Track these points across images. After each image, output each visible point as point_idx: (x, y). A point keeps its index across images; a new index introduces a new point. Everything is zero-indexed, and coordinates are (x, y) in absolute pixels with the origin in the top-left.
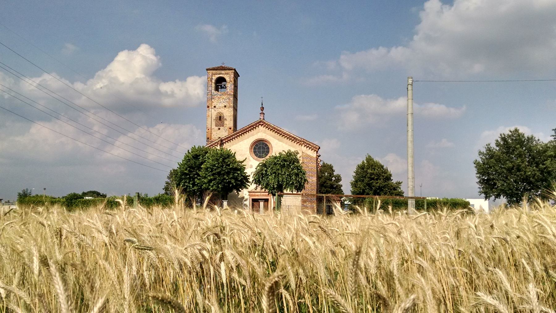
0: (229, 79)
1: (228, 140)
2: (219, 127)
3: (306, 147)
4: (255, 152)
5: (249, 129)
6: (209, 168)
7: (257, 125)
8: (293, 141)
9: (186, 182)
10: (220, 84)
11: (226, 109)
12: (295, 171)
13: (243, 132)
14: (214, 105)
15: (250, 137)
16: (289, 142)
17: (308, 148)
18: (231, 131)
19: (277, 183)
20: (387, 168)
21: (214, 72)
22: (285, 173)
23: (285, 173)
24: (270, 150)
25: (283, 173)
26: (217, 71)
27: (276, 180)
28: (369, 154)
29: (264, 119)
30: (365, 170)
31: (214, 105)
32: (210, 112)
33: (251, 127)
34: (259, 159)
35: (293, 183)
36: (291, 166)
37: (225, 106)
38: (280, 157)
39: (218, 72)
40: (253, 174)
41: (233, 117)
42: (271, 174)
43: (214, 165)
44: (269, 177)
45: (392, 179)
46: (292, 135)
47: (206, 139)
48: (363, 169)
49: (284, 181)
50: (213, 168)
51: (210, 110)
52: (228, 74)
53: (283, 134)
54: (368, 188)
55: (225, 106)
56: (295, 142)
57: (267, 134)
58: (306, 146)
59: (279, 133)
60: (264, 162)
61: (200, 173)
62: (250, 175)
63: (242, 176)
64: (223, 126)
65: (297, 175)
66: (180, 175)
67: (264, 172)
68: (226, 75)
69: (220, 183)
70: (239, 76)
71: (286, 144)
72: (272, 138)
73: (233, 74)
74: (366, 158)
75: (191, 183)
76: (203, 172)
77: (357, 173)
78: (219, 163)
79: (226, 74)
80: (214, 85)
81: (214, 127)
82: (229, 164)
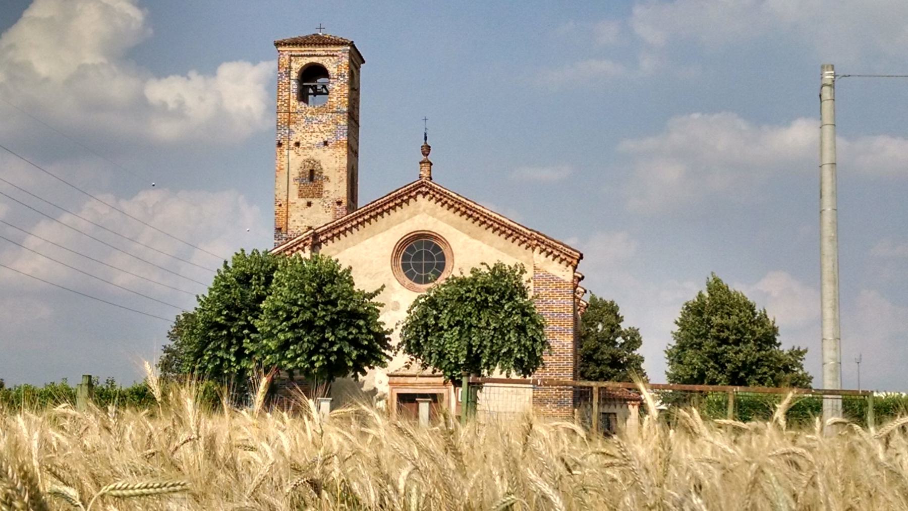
0: (336, 70)
2: (309, 200)
5: (391, 204)
6: (281, 309)
7: (413, 194)
8: (511, 239)
9: (219, 348)
10: (312, 84)
11: (329, 151)
12: (517, 319)
13: (373, 214)
15: (392, 225)
17: (551, 257)
18: (342, 209)
21: (296, 50)
22: (488, 324)
23: (488, 324)
25: (483, 324)
26: (303, 49)
27: (464, 342)
29: (431, 179)
30: (705, 316)
33: (395, 198)
34: (417, 285)
35: (510, 351)
37: (326, 143)
38: (475, 280)
39: (306, 50)
40: (400, 327)
41: (348, 172)
43: (294, 303)
45: (778, 342)
47: (273, 231)
48: (700, 313)
49: (485, 347)
51: (286, 152)
52: (333, 56)
53: (482, 219)
54: (712, 367)
56: (514, 241)
57: (440, 219)
58: (545, 250)
59: (470, 216)
61: (257, 323)
62: (392, 330)
63: (370, 332)
64: (319, 195)
65: (521, 329)
68: (327, 59)
70: (363, 62)
71: (491, 244)
72: (453, 230)
73: (347, 55)
75: (232, 350)
77: (683, 324)
79: (328, 55)
80: (296, 87)
81: (296, 198)
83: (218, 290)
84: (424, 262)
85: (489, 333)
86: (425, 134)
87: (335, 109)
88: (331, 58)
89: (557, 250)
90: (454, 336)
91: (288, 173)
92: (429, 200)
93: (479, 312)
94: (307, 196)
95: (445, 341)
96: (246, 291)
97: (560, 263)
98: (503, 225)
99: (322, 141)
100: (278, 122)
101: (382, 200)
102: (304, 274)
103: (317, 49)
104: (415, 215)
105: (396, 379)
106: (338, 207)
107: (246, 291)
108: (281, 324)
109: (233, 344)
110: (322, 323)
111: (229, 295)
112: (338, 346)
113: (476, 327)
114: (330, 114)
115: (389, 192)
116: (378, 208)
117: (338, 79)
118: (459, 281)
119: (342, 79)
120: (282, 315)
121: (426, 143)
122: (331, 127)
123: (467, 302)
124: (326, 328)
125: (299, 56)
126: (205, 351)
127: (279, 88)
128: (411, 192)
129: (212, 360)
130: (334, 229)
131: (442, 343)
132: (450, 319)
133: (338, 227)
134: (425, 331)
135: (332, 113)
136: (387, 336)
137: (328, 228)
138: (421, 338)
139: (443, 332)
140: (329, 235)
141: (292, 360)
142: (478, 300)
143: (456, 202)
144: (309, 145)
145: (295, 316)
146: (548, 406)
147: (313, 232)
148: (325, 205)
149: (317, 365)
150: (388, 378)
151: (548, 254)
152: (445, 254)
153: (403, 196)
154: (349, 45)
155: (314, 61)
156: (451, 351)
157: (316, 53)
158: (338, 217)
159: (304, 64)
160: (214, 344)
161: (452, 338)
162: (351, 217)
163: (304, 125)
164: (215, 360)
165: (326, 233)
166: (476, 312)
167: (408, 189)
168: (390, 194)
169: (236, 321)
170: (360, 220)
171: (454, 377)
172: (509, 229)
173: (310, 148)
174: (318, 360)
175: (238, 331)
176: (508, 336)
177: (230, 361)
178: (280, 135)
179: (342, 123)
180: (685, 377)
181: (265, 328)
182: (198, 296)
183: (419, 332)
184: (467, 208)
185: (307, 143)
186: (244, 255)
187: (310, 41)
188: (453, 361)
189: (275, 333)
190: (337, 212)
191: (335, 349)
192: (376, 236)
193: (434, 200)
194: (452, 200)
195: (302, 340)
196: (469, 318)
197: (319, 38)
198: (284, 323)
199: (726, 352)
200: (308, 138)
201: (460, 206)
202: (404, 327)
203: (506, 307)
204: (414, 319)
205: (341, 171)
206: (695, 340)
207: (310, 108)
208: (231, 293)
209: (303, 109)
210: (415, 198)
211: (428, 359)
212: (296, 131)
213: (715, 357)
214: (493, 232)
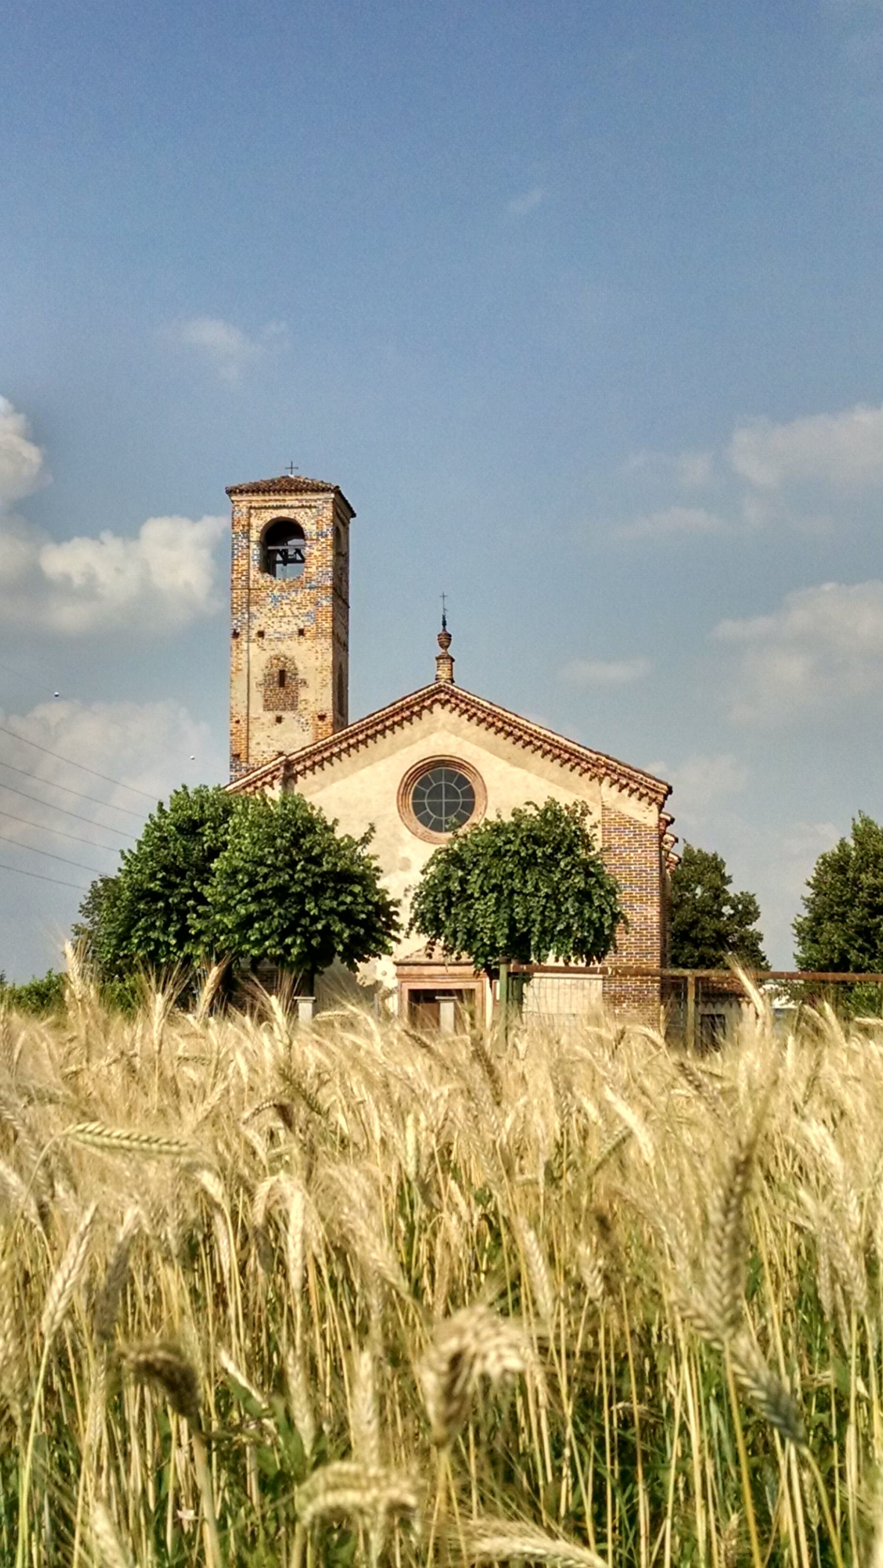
0: (314, 527)
1: (315, 763)
2: (279, 713)
3: (616, 787)
4: (418, 808)
6: (240, 870)
7: (428, 703)
9: (152, 927)
10: (281, 548)
11: (306, 644)
12: (579, 881)
13: (370, 732)
14: (257, 625)
15: (399, 748)
16: (552, 767)
17: (626, 792)
18: (326, 727)
19: (506, 931)
21: (257, 499)
22: (537, 889)
24: (478, 800)
25: (530, 888)
26: (267, 498)
27: (504, 915)
29: (453, 681)
30: (850, 874)
32: (245, 653)
33: (402, 709)
34: (435, 834)
35: (568, 927)
36: (558, 865)
37: (301, 632)
38: (518, 825)
39: (273, 499)
40: (411, 894)
41: (334, 673)
43: (261, 862)
44: (476, 906)
46: (561, 740)
47: (228, 758)
48: (842, 870)
49: (534, 921)
50: (257, 874)
51: (245, 646)
52: (310, 507)
55: (301, 632)
56: (572, 768)
57: (466, 738)
58: (617, 781)
59: (510, 734)
61: (207, 891)
63: (368, 902)
64: (293, 707)
67: (455, 886)
70: (354, 515)
71: (540, 774)
72: (485, 754)
73: (330, 506)
75: (171, 929)
77: (817, 885)
79: (303, 507)
80: (257, 552)
81: (261, 710)
82: (320, 856)
84: (444, 800)
86: (444, 617)
87: (313, 583)
88: (308, 510)
95: (476, 913)
97: (640, 799)
98: (556, 747)
99: (296, 629)
103: (287, 498)
106: (320, 723)
108: (240, 892)
112: (323, 922)
114: (307, 591)
116: (377, 724)
117: (318, 540)
119: (323, 540)
120: (242, 880)
121: (444, 630)
122: (308, 608)
124: (306, 896)
126: (133, 931)
127: (233, 554)
128: (423, 701)
133: (321, 752)
135: (310, 588)
141: (258, 943)
142: (523, 854)
143: (489, 714)
144: (277, 635)
146: (624, 1005)
148: (302, 720)
149: (295, 951)
150: (395, 967)
153: (412, 706)
154: (332, 491)
158: (320, 737)
161: (486, 910)
170: (352, 741)
172: (566, 752)
173: (279, 639)
175: (180, 902)
179: (325, 603)
181: (218, 898)
182: (122, 852)
184: (505, 722)
185: (275, 632)
186: (187, 794)
194: (483, 712)
195: (271, 914)
196: (509, 881)
205: (325, 673)
208: (169, 848)
210: (430, 708)
211: (451, 939)
212: (258, 615)
214: (543, 757)
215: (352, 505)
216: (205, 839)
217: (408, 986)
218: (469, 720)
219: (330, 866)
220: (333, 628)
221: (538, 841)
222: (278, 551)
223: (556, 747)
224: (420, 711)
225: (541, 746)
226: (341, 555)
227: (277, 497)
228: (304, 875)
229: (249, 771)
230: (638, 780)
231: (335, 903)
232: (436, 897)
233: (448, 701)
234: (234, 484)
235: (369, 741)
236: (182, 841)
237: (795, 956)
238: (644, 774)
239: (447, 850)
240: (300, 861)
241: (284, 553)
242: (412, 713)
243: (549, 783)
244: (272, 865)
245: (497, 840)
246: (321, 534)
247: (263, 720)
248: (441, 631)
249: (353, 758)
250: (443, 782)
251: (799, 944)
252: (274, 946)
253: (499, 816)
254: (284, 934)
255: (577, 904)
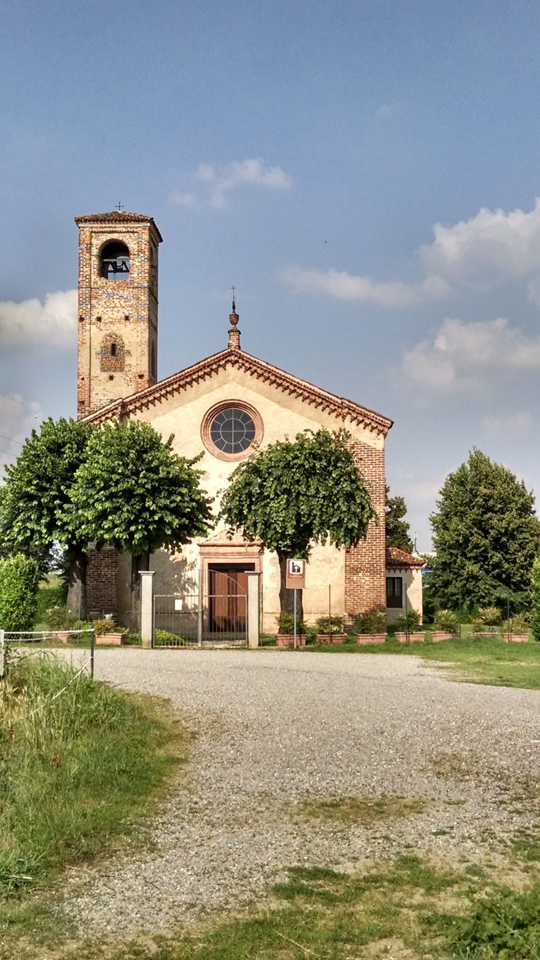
0: (136, 246)
1: (142, 404)
2: (112, 373)
3: (355, 422)
4: (215, 437)
5: (200, 373)
6: (98, 477)
7: (222, 363)
8: (321, 407)
9: (29, 519)
10: (113, 260)
11: (130, 326)
12: (346, 486)
13: (182, 383)
14: (96, 313)
15: (201, 394)
16: (309, 409)
17: (362, 426)
18: (144, 382)
19: (294, 523)
20: (523, 482)
21: (97, 226)
22: (318, 491)
23: (318, 491)
24: (258, 431)
25: (312, 491)
26: (104, 225)
27: (292, 512)
28: (478, 448)
29: (240, 348)
30: (469, 487)
31: (96, 313)
32: (88, 332)
33: (204, 367)
34: (227, 455)
35: (340, 520)
36: (330, 473)
37: (127, 318)
38: (302, 445)
39: (107, 226)
40: (221, 495)
41: (149, 346)
42: (277, 495)
43: (113, 471)
44: (272, 504)
45: (533, 509)
46: (316, 389)
47: (76, 404)
48: (462, 484)
49: (315, 516)
50: (111, 479)
51: (88, 327)
52: (133, 232)
53: (292, 387)
54: (476, 532)
55: (127, 318)
56: (324, 409)
57: (250, 388)
58: (356, 418)
59: (280, 385)
60: (254, 462)
61: (71, 493)
62: (214, 499)
63: (192, 500)
64: (122, 369)
65: (350, 497)
66: (13, 500)
67: (256, 490)
68: (128, 235)
69: (135, 522)
70: (161, 241)
71: (301, 413)
72: (262, 399)
73: (147, 231)
74: (471, 457)
75: (43, 521)
76: (81, 490)
77: (446, 494)
78: (126, 465)
79: (128, 232)
80: (97, 263)
81: (99, 372)
82: (157, 468)
83: (27, 459)
84: (233, 431)
85: (318, 501)
86: (234, 304)
87: (136, 285)
88: (132, 235)
89: (369, 418)
90: (281, 505)
91: (90, 347)
92: (238, 369)
93: (307, 480)
94: (109, 370)
95: (271, 510)
96: (58, 460)
97: (371, 431)
98: (313, 394)
99: (123, 316)
100: (79, 298)
101: (192, 369)
102: (121, 441)
103: (117, 226)
104: (225, 384)
105: (207, 549)
106: (139, 380)
107: (58, 460)
108: (98, 493)
109: (44, 515)
110: (142, 491)
111: (39, 465)
112: (159, 515)
113: (305, 494)
114: (131, 290)
115: (199, 361)
116: (187, 377)
117: (138, 255)
118: (285, 447)
119: (142, 255)
120: (99, 484)
121: (234, 312)
122: (132, 302)
123: (294, 470)
124: (146, 496)
125: (100, 232)
126: (14, 522)
127: (80, 264)
128: (219, 361)
129: (22, 531)
130: (143, 398)
131: (268, 513)
132: (276, 487)
133: (147, 396)
134: (248, 500)
135: (133, 288)
136: (207, 505)
137: (137, 398)
138: (244, 508)
139: (268, 500)
140: (138, 404)
141: (109, 530)
142: (306, 467)
143: (266, 371)
144: (110, 320)
145: (113, 484)
146: (360, 574)
147: (122, 402)
148: (127, 378)
149: (137, 536)
150: (199, 548)
151: (360, 422)
152: (254, 422)
153: (212, 365)
154: (149, 222)
155: (115, 238)
156: (278, 520)
157: (116, 230)
158: (140, 390)
159: (105, 240)
160: (24, 515)
161: (279, 508)
162: (160, 386)
163: (105, 300)
164: (25, 532)
165: (135, 402)
166: (305, 479)
167: (217, 358)
168: (199, 363)
169: (47, 491)
170: (169, 389)
171: (280, 548)
172: (319, 397)
173: (111, 323)
174: (137, 530)
175: (50, 501)
176: (337, 505)
177: (40, 533)
178: (81, 310)
179: (143, 298)
180: (451, 542)
181: (81, 497)
182: (6, 466)
183: (242, 501)
184: (277, 377)
185: (109, 318)
186: (53, 424)
187: (111, 218)
188: (280, 531)
189: (91, 503)
190: (139, 386)
191: (156, 518)
192: (186, 405)
193: (243, 369)
194: (262, 369)
195: (121, 509)
196: (297, 486)
197: (120, 215)
198: (102, 492)
199: (491, 519)
200: (110, 313)
201: (270, 375)
202: (225, 495)
203: (334, 475)
204: (236, 488)
205: (143, 346)
206: (459, 508)
207: (111, 283)
208: (41, 462)
209: (104, 285)
210: (224, 367)
211: (252, 529)
212: (97, 306)
213: (478, 523)
214: (303, 401)
215: (161, 233)
216: (65, 456)
217: (207, 561)
218: (251, 375)
219: (165, 473)
220: (149, 315)
221: (316, 457)
222: (110, 262)
223: (313, 394)
224: (217, 368)
225: (302, 394)
226: (154, 267)
227: (110, 225)
228: (146, 480)
229: (90, 413)
230: (371, 417)
231: (168, 502)
232: (240, 497)
233: (237, 362)
234: (80, 215)
235: (181, 389)
236: (51, 457)
237: (433, 539)
238: (375, 413)
239: (248, 464)
240: (143, 470)
241: (114, 264)
242: (212, 369)
243: (307, 419)
244: (122, 474)
245: (287, 456)
246: (140, 251)
247: (100, 378)
248: (231, 312)
249: (169, 401)
250: (233, 419)
251: (434, 530)
252: (121, 532)
253: (287, 439)
254: (129, 523)
255: (346, 503)
